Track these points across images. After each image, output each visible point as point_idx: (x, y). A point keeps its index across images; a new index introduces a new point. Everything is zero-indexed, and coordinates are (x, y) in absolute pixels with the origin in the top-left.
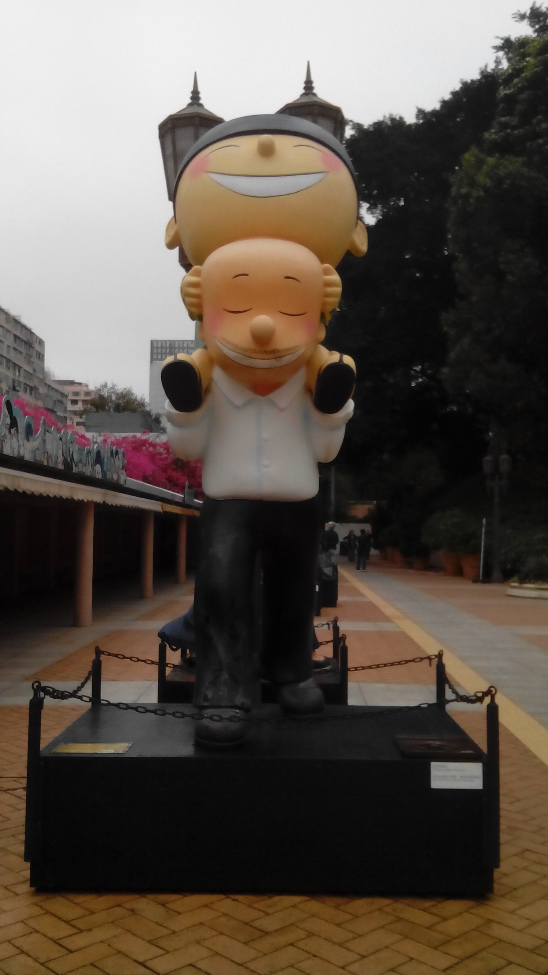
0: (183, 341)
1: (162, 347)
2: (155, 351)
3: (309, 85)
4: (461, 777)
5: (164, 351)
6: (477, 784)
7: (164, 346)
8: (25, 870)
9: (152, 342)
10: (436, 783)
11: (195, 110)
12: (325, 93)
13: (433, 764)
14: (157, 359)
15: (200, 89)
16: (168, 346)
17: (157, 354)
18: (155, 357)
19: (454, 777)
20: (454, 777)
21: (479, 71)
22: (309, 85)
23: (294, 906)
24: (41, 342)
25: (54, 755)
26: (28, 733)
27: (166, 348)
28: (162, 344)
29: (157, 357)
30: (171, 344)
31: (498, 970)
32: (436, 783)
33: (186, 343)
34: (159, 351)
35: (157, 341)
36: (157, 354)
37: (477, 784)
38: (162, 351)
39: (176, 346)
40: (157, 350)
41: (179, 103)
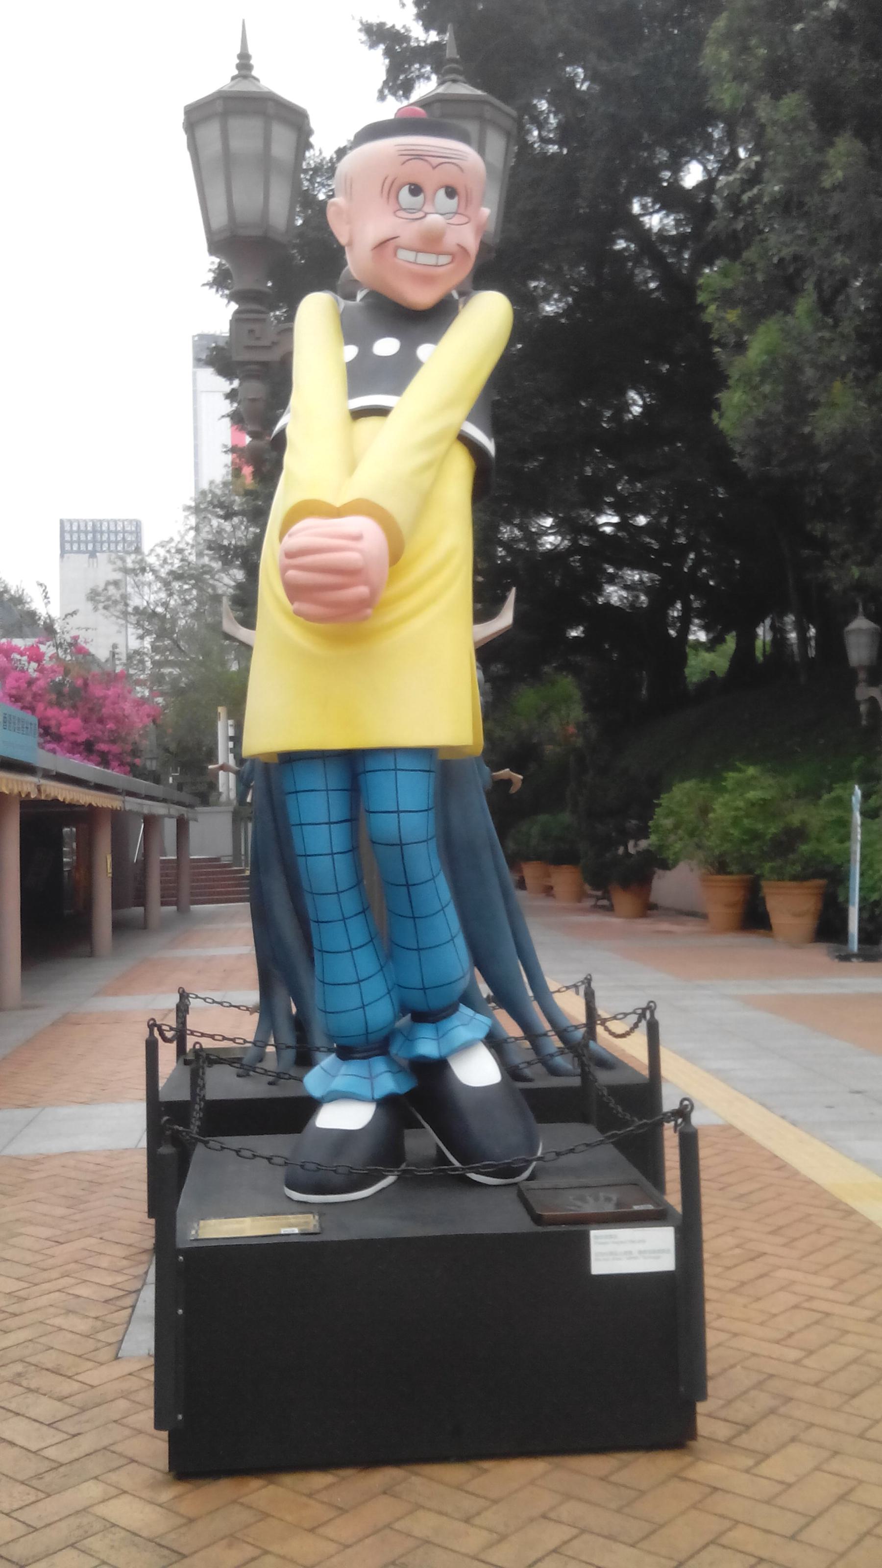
0: (115, 522)
1: (79, 531)
2: (67, 537)
3: (244, 64)
4: (640, 1252)
5: (83, 537)
6: (666, 1263)
7: (112, 528)
8: (156, 1447)
9: (62, 522)
10: (599, 1266)
11: (244, 86)
12: (271, 78)
13: (593, 1233)
14: (72, 551)
15: (251, 51)
16: (89, 528)
17: (72, 543)
18: (68, 547)
19: (629, 1254)
20: (629, 1254)
21: (372, 50)
22: (244, 64)
23: (532, 1482)
24: (185, 107)
25: (195, 1244)
26: (146, 1209)
27: (86, 533)
28: (79, 526)
29: (87, 547)
30: (94, 526)
31: (535, 1563)
32: (599, 1266)
33: (90, 524)
34: (75, 538)
35: (71, 522)
36: (72, 543)
37: (666, 1263)
38: (94, 537)
39: (119, 529)
40: (71, 537)
41: (219, 77)
